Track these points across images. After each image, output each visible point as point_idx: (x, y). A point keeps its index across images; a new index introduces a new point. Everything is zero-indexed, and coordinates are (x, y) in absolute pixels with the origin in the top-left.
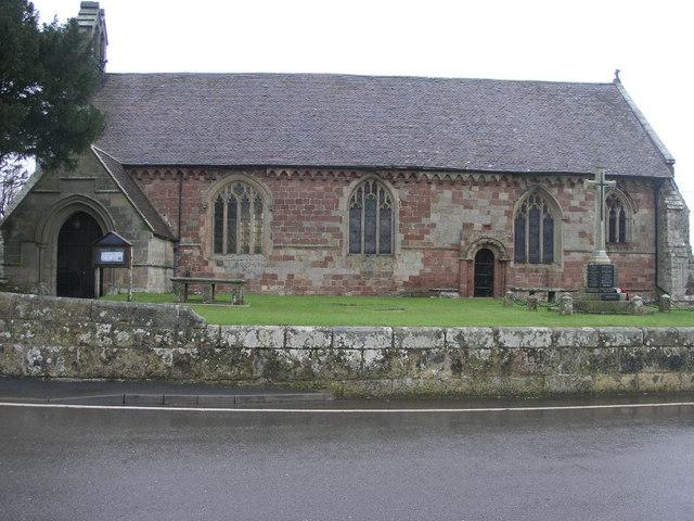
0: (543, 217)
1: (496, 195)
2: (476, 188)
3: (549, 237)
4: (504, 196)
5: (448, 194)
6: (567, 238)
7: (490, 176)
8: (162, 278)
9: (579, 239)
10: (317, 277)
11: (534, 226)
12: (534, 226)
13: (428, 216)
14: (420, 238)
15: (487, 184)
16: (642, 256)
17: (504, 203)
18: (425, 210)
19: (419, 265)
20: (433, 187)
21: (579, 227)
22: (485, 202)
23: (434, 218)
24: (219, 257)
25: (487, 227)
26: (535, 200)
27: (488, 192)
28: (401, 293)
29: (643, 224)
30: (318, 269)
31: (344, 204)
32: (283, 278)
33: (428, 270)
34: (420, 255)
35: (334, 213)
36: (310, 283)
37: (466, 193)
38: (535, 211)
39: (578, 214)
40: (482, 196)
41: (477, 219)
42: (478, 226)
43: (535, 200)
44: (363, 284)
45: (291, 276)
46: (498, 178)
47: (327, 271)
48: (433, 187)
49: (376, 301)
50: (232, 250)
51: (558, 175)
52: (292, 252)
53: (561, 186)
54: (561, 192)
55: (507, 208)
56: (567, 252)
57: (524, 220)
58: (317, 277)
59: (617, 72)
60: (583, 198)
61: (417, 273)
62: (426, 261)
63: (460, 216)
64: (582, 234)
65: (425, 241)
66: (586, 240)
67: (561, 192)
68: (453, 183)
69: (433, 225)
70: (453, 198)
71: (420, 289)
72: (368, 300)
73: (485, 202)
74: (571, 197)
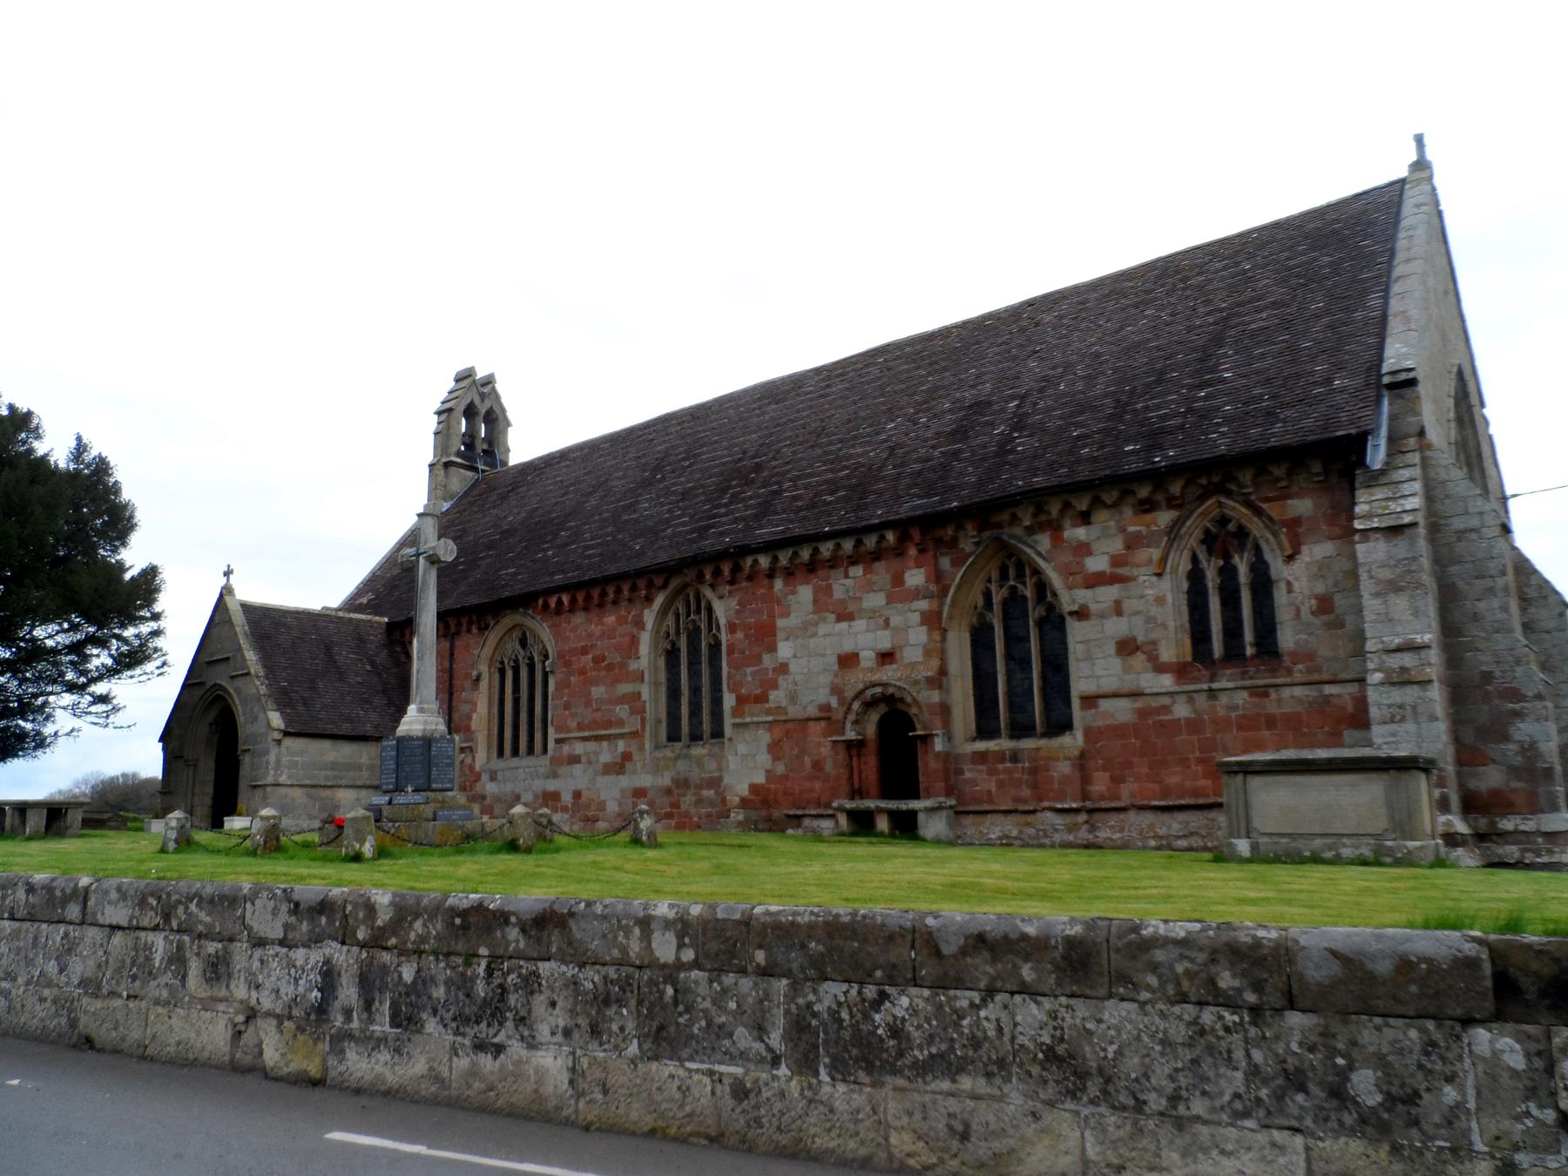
0: (1034, 613)
1: (898, 580)
2: (857, 571)
3: (1057, 667)
4: (915, 577)
5: (805, 593)
6: (1094, 667)
7: (830, 545)
8: (1440, 746)
9: (1117, 663)
10: (611, 792)
11: (1015, 640)
12: (1015, 640)
13: (772, 648)
14: (762, 698)
15: (876, 556)
16: (1328, 689)
17: (917, 594)
18: (765, 636)
19: (764, 759)
20: (779, 584)
21: (1117, 627)
22: (876, 600)
23: (785, 650)
24: (498, 764)
25: (886, 657)
26: (1012, 573)
27: (882, 572)
28: (740, 824)
29: (1320, 588)
30: (610, 779)
31: (646, 654)
32: (567, 798)
33: (780, 769)
34: (765, 737)
35: (633, 666)
36: (602, 806)
37: (842, 585)
38: (1014, 604)
39: (1107, 594)
40: (870, 587)
41: (865, 638)
42: (868, 658)
43: (1012, 573)
44: (676, 805)
45: (577, 795)
46: (891, 537)
47: (625, 781)
48: (779, 584)
49: (701, 836)
50: (696, 737)
51: (1036, 498)
52: (579, 748)
53: (1055, 528)
54: (1057, 539)
55: (924, 605)
56: (1089, 701)
57: (992, 628)
58: (611, 792)
59: (1419, 140)
60: (1117, 545)
61: (760, 779)
62: (774, 748)
63: (836, 636)
64: (1127, 647)
65: (771, 705)
66: (1139, 660)
67: (1057, 539)
68: (812, 567)
69: (783, 668)
70: (815, 601)
71: (773, 813)
72: (685, 836)
73: (876, 600)
74: (1084, 549)
